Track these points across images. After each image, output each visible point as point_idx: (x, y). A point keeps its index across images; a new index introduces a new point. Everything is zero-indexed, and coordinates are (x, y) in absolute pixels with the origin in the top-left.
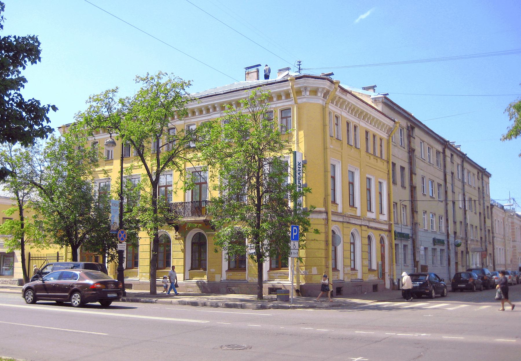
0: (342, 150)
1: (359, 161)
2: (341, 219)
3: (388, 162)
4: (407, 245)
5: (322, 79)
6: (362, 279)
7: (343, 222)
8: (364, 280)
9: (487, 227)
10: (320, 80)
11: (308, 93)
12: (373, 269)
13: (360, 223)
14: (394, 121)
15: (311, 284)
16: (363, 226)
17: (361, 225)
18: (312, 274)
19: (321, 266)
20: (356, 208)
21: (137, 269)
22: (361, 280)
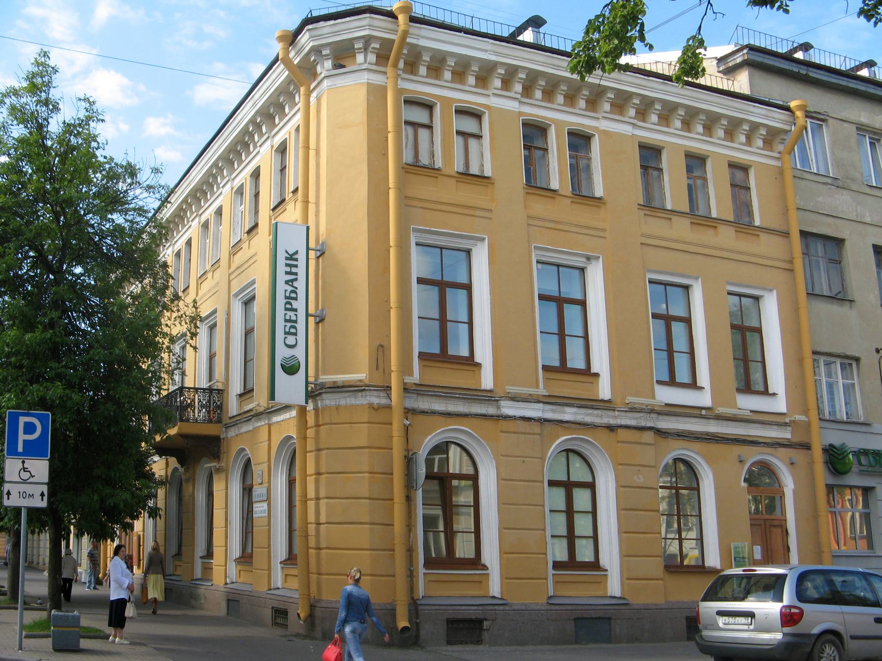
3: (786, 234)
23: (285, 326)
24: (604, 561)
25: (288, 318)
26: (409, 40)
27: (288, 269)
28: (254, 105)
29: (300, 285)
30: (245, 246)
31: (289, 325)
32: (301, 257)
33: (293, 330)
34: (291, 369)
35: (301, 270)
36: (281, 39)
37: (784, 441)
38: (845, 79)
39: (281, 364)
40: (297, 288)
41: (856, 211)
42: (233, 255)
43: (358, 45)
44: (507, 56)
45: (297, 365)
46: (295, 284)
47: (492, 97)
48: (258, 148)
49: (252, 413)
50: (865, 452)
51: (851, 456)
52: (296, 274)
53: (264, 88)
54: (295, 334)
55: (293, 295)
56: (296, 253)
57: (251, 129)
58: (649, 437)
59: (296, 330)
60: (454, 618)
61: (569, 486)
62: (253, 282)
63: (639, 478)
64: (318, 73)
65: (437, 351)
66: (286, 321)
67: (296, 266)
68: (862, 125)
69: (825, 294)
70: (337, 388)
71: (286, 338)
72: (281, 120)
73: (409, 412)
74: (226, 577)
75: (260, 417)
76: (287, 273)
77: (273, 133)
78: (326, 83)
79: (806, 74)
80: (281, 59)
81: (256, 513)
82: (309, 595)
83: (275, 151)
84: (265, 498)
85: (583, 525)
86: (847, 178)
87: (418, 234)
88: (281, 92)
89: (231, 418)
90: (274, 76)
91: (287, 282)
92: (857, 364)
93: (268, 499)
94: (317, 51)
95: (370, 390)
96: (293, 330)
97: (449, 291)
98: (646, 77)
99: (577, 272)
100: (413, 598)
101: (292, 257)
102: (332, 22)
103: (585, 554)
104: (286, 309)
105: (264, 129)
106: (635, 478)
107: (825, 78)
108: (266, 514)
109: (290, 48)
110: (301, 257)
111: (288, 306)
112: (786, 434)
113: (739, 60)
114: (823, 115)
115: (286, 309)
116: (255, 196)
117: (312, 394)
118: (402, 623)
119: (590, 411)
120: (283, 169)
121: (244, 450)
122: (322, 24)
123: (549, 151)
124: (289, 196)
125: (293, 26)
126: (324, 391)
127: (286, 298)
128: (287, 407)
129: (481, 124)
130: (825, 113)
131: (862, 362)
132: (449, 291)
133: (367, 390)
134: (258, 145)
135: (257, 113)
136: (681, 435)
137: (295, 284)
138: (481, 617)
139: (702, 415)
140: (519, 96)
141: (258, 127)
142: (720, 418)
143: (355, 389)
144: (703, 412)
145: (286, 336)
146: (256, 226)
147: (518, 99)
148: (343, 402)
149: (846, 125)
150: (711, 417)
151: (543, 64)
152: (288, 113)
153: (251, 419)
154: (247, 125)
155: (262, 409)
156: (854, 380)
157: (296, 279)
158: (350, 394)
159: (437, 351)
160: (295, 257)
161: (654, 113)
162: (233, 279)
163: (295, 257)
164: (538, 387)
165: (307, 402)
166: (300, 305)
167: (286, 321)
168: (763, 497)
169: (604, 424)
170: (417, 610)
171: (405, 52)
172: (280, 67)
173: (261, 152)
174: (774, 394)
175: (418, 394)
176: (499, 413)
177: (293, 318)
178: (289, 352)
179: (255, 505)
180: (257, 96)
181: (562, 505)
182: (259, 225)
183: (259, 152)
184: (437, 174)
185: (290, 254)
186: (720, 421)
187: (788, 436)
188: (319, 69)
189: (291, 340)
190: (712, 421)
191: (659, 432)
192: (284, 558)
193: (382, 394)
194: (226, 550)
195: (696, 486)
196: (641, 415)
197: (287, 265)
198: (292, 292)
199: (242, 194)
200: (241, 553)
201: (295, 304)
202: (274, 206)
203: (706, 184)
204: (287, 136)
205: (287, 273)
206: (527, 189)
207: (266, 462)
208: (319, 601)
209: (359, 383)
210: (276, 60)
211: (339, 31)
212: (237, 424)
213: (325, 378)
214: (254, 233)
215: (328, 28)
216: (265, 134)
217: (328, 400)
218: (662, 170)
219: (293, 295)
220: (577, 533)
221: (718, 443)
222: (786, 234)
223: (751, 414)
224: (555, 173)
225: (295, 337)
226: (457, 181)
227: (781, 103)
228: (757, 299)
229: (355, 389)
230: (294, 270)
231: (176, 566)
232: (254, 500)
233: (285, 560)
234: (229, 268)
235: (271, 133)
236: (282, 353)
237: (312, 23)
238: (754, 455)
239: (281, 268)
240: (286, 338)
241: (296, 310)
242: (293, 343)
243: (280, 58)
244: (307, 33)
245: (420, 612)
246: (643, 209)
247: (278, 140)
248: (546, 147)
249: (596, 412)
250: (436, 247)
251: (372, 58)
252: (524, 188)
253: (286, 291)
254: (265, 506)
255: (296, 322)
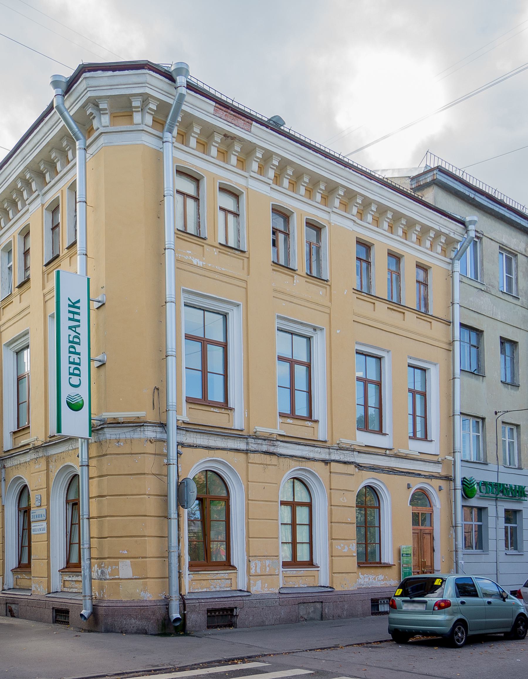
0: (248, 275)
1: (328, 311)
2: (241, 445)
3: (449, 323)
4: (485, 508)
5: (132, 69)
6: (331, 588)
7: (246, 452)
8: (336, 590)
9: (174, 100)
10: (126, 72)
11: (105, 119)
12: (384, 563)
13: (327, 457)
14: (463, 223)
15: (117, 601)
16: (333, 464)
17: (326, 462)
18: (119, 579)
19: (142, 558)
20: (316, 421)
21: (476, 547)
22: (330, 590)
23: (70, 367)
24: (317, 560)
25: (72, 360)
26: (184, 107)
27: (71, 316)
28: (24, 159)
29: (83, 330)
30: (16, 300)
31: (73, 366)
32: (83, 305)
33: (76, 372)
34: (75, 407)
35: (83, 317)
36: (55, 84)
37: (437, 474)
38: (498, 206)
39: (67, 401)
40: (79, 334)
41: (493, 311)
42: (48, 274)
43: (136, 103)
44: (265, 140)
45: (81, 403)
46: (78, 330)
47: (249, 179)
48: (27, 206)
49: (28, 447)
50: (484, 484)
51: (476, 486)
52: (79, 321)
53: (35, 141)
54: (79, 375)
55: (76, 340)
56: (78, 301)
57: (19, 185)
58: (351, 469)
59: (80, 371)
60: (213, 608)
61: (293, 505)
62: (26, 333)
63: (343, 499)
64: (95, 128)
65: (199, 396)
66: (70, 363)
67: (78, 314)
68: (503, 245)
69: (466, 370)
70: (116, 424)
71: (70, 378)
72: (52, 178)
73: (180, 444)
74: (3, 584)
75: (38, 450)
76: (70, 319)
77: (43, 191)
78: (102, 140)
79: (473, 198)
80: (56, 107)
81: (34, 530)
82: (92, 596)
83: (46, 209)
84: (45, 518)
85: (302, 535)
86: (489, 285)
87: (187, 295)
88: (53, 148)
89: (5, 452)
90: (45, 129)
91: (70, 328)
92: (482, 421)
93: (47, 519)
94: (94, 104)
95: (148, 426)
96: (76, 372)
97: (210, 347)
98: (369, 180)
99: (305, 340)
100: (181, 595)
101: (73, 305)
102: (110, 73)
103: (303, 555)
104: (70, 352)
105: (34, 186)
106: (341, 499)
107: (485, 203)
108: (45, 531)
109: (66, 97)
110: (83, 305)
111: (72, 350)
112: (438, 469)
113: (428, 180)
114: (480, 233)
115: (70, 352)
116: (24, 254)
117: (93, 430)
118: (175, 615)
119: (312, 448)
120: (55, 227)
121: (20, 478)
122: (99, 73)
123: (290, 235)
124: (63, 252)
125: (68, 73)
126: (105, 426)
127: (70, 342)
128: (70, 439)
129: (238, 204)
130: (481, 232)
131: (486, 420)
132: (210, 347)
133: (145, 426)
134: (27, 202)
135: (27, 167)
136: (373, 468)
137: (78, 330)
138: (232, 606)
139: (386, 454)
140: (271, 182)
141: (27, 184)
142: (397, 456)
143: (135, 425)
144: (388, 452)
145: (71, 376)
146: (27, 280)
147: (270, 184)
148: (122, 436)
149: (493, 243)
150: (392, 456)
151: (293, 154)
152: (60, 172)
153: (28, 452)
154: (15, 180)
155: (39, 443)
156: (479, 433)
157: (79, 326)
158: (131, 429)
159: (199, 396)
160: (76, 305)
161: (370, 213)
162: (4, 330)
163: (76, 305)
164: (276, 429)
165: (90, 436)
166: (82, 349)
167: (70, 363)
168: (420, 514)
169: (322, 458)
170: (184, 604)
171: (179, 119)
172: (55, 115)
173: (30, 211)
174: (431, 441)
175: (186, 431)
176: (248, 448)
177: (77, 361)
178: (73, 391)
179: (32, 524)
180: (26, 150)
181: (288, 519)
182: (31, 279)
183: (28, 210)
184: (203, 243)
185: (73, 302)
186: (398, 459)
187: (439, 471)
188: (95, 124)
189: (75, 380)
190: (393, 459)
191: (359, 466)
192: (63, 567)
193: (159, 429)
194: (49, 564)
195: (378, 505)
196: (347, 452)
197: (70, 312)
198: (75, 337)
199: (10, 252)
200: (17, 564)
201: (78, 348)
202: (47, 262)
203: (399, 278)
204: (59, 194)
205: (70, 319)
206: (273, 266)
207: (44, 488)
208: (101, 600)
209: (138, 420)
210: (51, 108)
211: (118, 85)
212: (12, 457)
213: (108, 415)
214: (25, 286)
215: (106, 79)
216: (35, 191)
217: (110, 434)
218: (370, 263)
219: (76, 340)
220: (298, 541)
221: (395, 474)
222: (449, 323)
223: (419, 454)
224: (295, 255)
225: (79, 378)
226: (219, 252)
227: (459, 217)
228: (424, 370)
229: (135, 425)
230: (76, 317)
231: (64, 581)
232: (32, 520)
233: (16, 568)
234: (44, 288)
235: (41, 191)
236: (67, 391)
237: (89, 71)
238: (417, 484)
239: (65, 315)
240: (70, 378)
241: (79, 354)
242: (78, 383)
243: (54, 106)
244: (84, 82)
245: (187, 605)
246: (356, 293)
247: (49, 198)
248: (288, 232)
249: (317, 449)
250: (200, 309)
251: (149, 119)
252: (271, 265)
253: (69, 335)
254: (44, 524)
255: (79, 364)
